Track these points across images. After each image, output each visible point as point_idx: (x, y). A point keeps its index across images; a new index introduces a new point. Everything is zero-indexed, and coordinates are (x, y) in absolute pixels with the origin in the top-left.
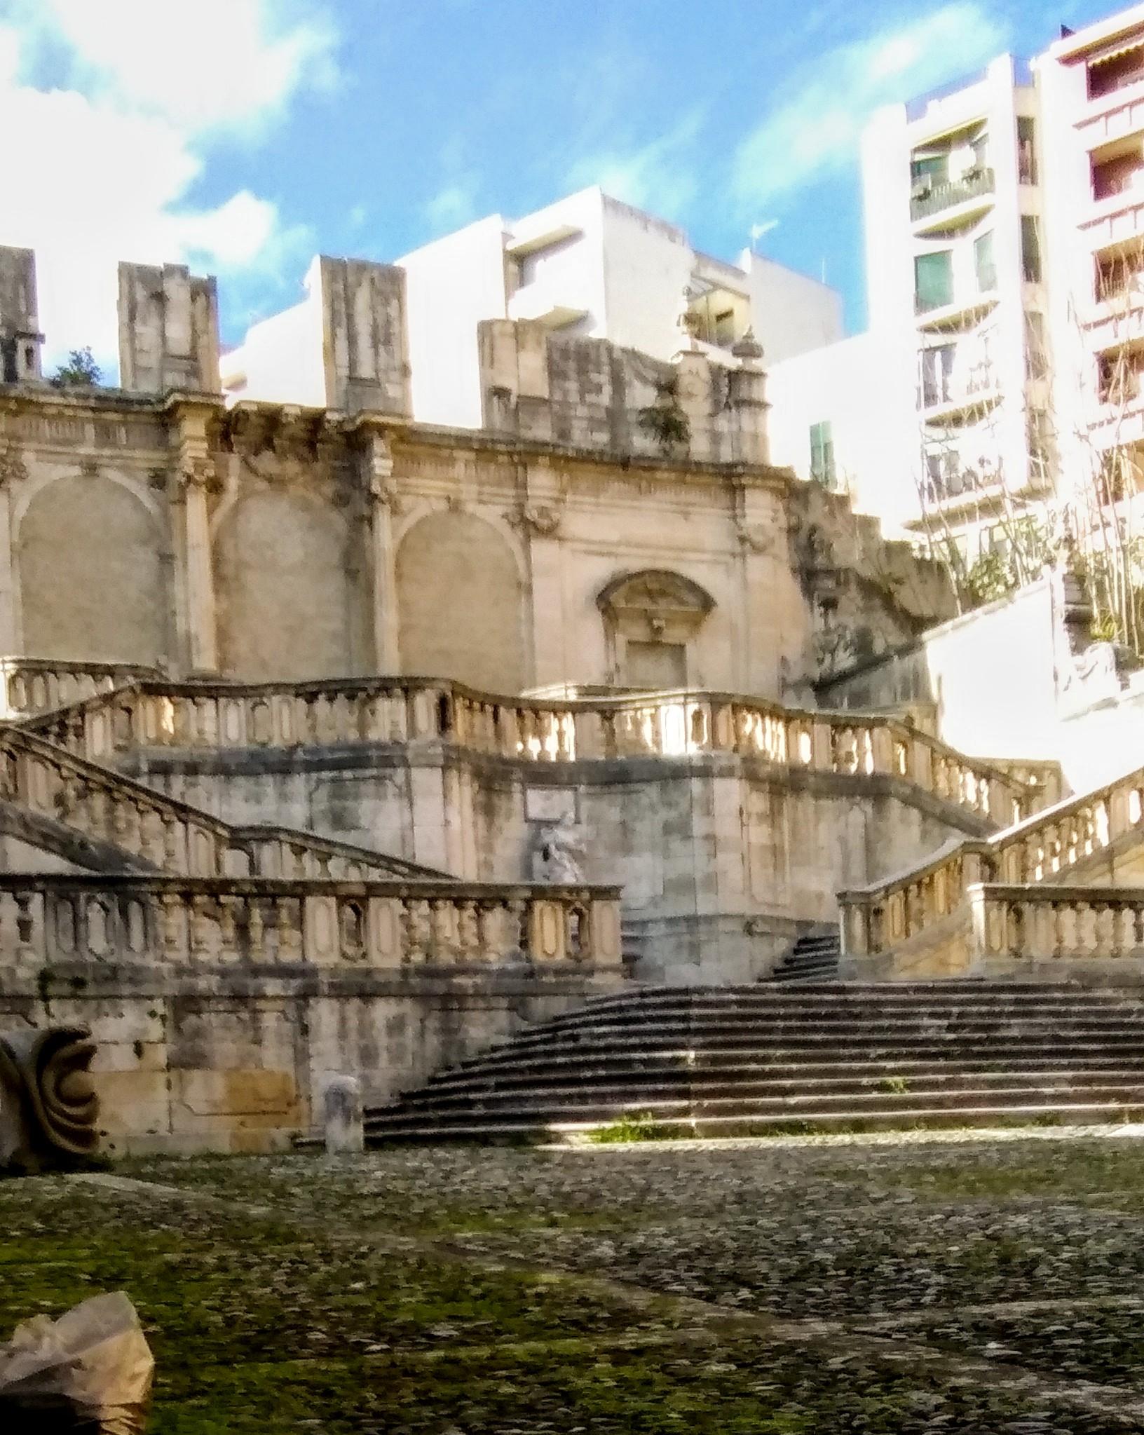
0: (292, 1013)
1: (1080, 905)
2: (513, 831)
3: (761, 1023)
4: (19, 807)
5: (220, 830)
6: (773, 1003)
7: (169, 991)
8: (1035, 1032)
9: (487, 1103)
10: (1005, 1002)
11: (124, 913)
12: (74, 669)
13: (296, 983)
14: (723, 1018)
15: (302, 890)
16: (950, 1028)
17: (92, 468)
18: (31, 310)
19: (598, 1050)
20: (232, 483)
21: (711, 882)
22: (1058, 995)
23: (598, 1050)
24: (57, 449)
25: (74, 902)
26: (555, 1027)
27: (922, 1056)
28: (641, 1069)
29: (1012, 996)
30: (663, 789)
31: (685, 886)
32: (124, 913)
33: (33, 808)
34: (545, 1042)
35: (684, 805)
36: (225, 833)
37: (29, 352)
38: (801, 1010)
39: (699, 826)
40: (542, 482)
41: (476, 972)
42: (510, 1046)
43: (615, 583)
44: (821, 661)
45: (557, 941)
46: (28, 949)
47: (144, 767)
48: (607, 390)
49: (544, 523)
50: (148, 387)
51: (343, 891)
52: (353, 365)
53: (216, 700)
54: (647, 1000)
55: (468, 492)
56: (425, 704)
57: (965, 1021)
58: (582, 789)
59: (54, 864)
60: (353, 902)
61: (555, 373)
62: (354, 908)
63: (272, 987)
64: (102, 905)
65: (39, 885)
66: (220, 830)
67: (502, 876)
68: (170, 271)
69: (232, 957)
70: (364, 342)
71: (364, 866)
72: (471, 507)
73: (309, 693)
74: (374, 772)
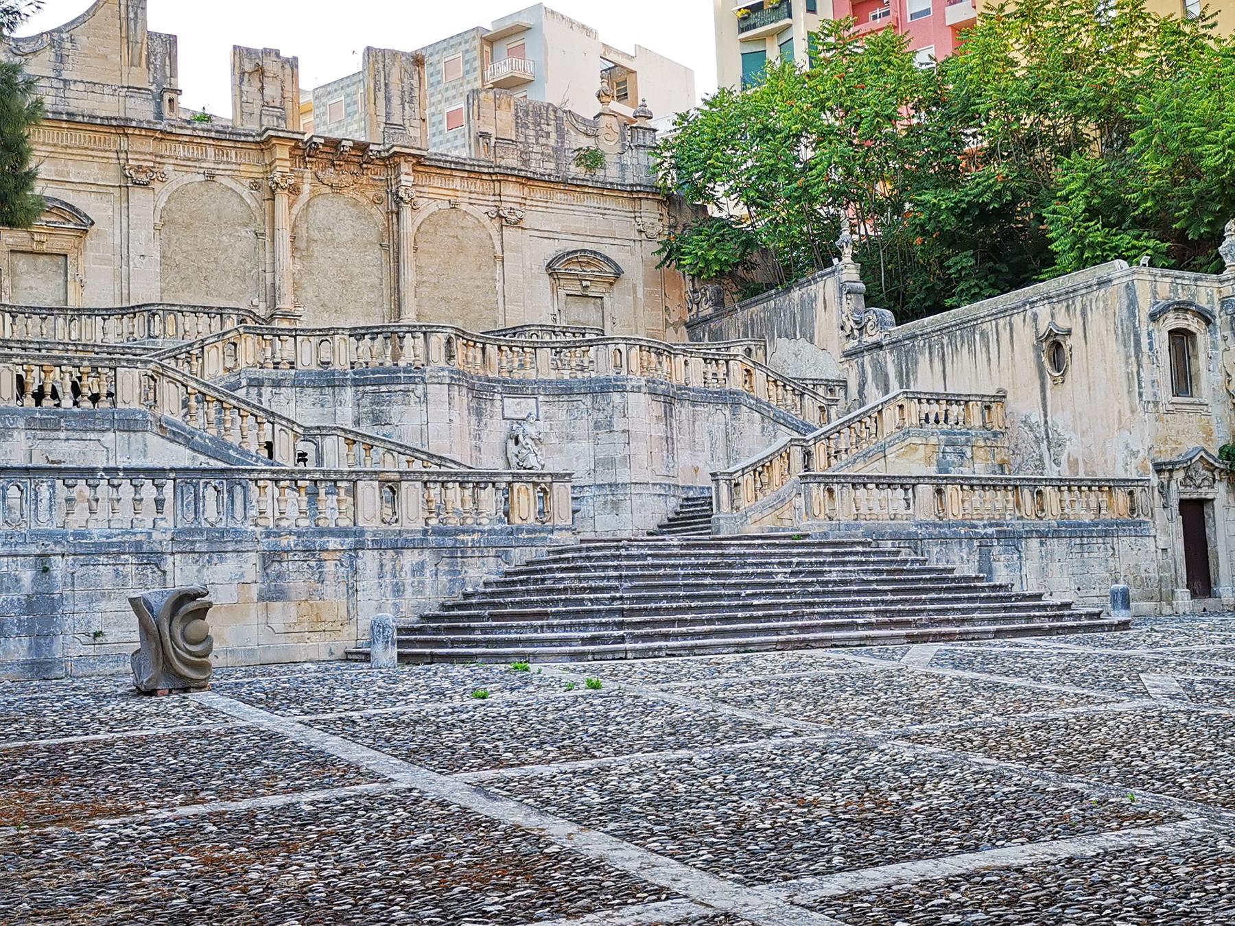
0: (346, 563)
1: (869, 486)
2: (496, 430)
3: (669, 571)
4: (158, 412)
5: (296, 428)
6: (675, 556)
7: (260, 547)
8: (848, 577)
9: (484, 630)
10: (826, 554)
11: (231, 492)
12: (195, 310)
13: (350, 540)
14: (643, 567)
15: (354, 478)
16: (792, 574)
17: (211, 177)
18: (174, 74)
19: (559, 591)
20: (306, 188)
21: (627, 460)
22: (860, 549)
23: (559, 591)
24: (185, 165)
25: (196, 486)
26: (531, 569)
27: (777, 594)
28: (589, 607)
29: (830, 550)
30: (594, 399)
31: (610, 463)
32: (231, 492)
33: (167, 414)
34: (522, 582)
35: (609, 410)
36: (300, 431)
37: (171, 101)
38: (693, 561)
39: (618, 424)
40: (511, 191)
41: (474, 532)
42: (497, 583)
43: (556, 259)
44: (690, 310)
45: (529, 511)
46: (162, 519)
47: (244, 383)
48: (554, 136)
49: (512, 218)
50: (253, 126)
51: (383, 477)
52: (388, 115)
53: (295, 337)
54: (591, 554)
55: (463, 198)
56: (438, 341)
57: (801, 568)
58: (541, 398)
59: (181, 457)
60: (390, 484)
61: (520, 125)
62: (391, 488)
63: (333, 543)
64: (215, 488)
65: (172, 475)
66: (296, 428)
67: (491, 462)
68: (267, 52)
69: (304, 523)
70: (396, 101)
71: (395, 454)
72: (463, 207)
73: (358, 334)
74: (402, 387)
